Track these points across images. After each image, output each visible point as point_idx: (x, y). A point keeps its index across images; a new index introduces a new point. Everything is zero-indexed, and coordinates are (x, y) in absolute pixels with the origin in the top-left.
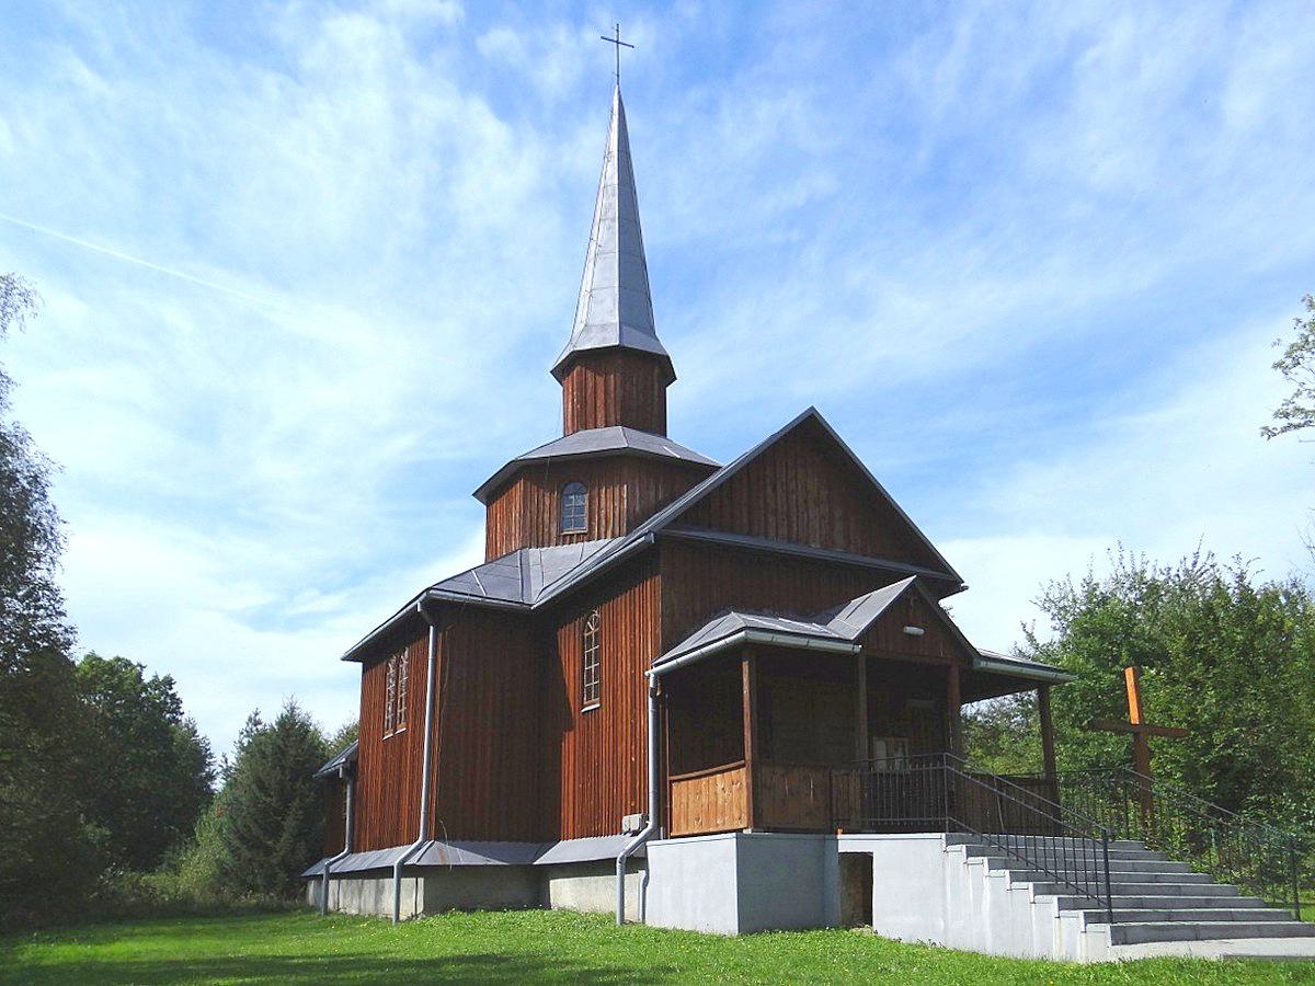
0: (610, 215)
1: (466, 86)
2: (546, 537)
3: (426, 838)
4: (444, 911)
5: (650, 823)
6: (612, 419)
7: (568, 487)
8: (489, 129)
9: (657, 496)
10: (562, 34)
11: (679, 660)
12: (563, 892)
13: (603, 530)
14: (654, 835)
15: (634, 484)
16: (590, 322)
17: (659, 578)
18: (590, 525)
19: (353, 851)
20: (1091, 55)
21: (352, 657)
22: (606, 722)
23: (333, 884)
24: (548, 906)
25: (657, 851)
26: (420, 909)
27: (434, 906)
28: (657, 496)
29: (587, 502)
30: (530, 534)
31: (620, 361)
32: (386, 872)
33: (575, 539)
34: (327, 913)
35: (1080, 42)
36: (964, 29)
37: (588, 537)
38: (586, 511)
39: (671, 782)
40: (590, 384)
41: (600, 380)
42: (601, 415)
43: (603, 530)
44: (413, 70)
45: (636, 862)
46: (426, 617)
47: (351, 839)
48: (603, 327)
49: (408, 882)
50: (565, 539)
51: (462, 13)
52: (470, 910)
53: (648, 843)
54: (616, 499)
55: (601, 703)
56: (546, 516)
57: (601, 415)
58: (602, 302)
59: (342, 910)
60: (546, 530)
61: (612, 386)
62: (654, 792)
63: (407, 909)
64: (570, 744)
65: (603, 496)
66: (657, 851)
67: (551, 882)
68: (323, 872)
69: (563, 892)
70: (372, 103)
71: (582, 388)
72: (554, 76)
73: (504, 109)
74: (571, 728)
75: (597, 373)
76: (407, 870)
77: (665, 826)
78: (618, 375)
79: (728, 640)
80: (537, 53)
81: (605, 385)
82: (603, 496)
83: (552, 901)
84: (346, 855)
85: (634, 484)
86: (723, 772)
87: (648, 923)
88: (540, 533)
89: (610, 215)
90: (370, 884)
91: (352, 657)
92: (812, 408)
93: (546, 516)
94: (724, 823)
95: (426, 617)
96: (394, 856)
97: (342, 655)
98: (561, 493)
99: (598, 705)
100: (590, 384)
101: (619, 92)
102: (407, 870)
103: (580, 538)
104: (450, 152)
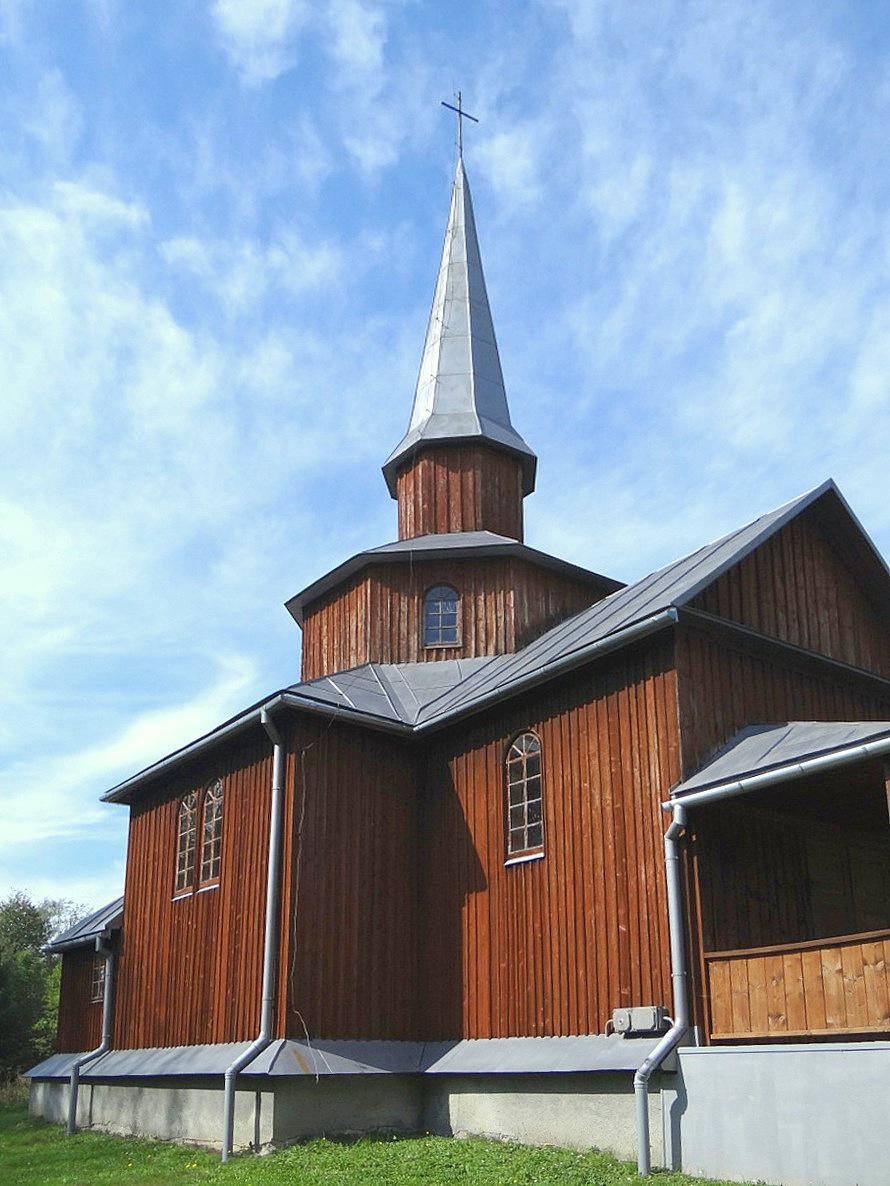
0: (458, 295)
1: (147, 292)
2: (403, 651)
3: (273, 1036)
4: (303, 1140)
5: (678, 1023)
6: (453, 526)
7: (433, 591)
8: (172, 336)
9: (547, 611)
10: (247, 250)
11: (805, 764)
12: (472, 1113)
13: (482, 645)
14: (685, 1038)
15: (521, 592)
16: (437, 411)
17: (672, 677)
18: (464, 638)
19: (110, 1047)
20: (742, 325)
21: (118, 797)
22: (557, 879)
23: (84, 1090)
24: (447, 1132)
25: (694, 1062)
26: (267, 1136)
27: (292, 1133)
28: (547, 611)
29: (459, 612)
30: (382, 647)
31: (480, 457)
32: (212, 1081)
33: (444, 655)
34: (75, 1130)
35: (735, 313)
36: (631, 290)
37: (463, 652)
38: (458, 621)
39: (707, 961)
40: (442, 482)
41: (455, 477)
42: (456, 518)
43: (482, 645)
44: (94, 271)
45: (665, 1075)
46: (272, 732)
47: (111, 1030)
48: (456, 417)
49: (245, 1097)
50: (427, 654)
51: (147, 217)
52: (348, 1140)
53: (680, 1050)
54: (499, 609)
55: (546, 851)
56: (404, 626)
57: (456, 518)
58: (452, 389)
59: (96, 1127)
60: (403, 642)
61: (471, 484)
62: (268, 1000)
63: (243, 1138)
64: (478, 916)
65: (481, 603)
66: (694, 1062)
67: (452, 1097)
68: (70, 1074)
69: (472, 1113)
70: (47, 299)
71: (430, 485)
72: (238, 290)
73: (185, 316)
74: (480, 883)
75: (451, 468)
76: (243, 1080)
77: (701, 1025)
78: (479, 472)
79: (869, 746)
80: (221, 266)
81: (462, 484)
82: (481, 603)
83: (453, 1123)
84: (102, 1052)
85: (521, 592)
86: (838, 946)
87: (689, 1168)
88: (396, 646)
89: (458, 295)
90: (162, 1095)
91: (118, 797)
92: (831, 479)
93: (404, 626)
94: (845, 1023)
95: (272, 732)
96: (222, 1058)
97: (103, 795)
98: (423, 597)
99: (541, 855)
100: (442, 482)
101: (462, 165)
102: (243, 1080)
103: (451, 653)
104: (126, 354)
